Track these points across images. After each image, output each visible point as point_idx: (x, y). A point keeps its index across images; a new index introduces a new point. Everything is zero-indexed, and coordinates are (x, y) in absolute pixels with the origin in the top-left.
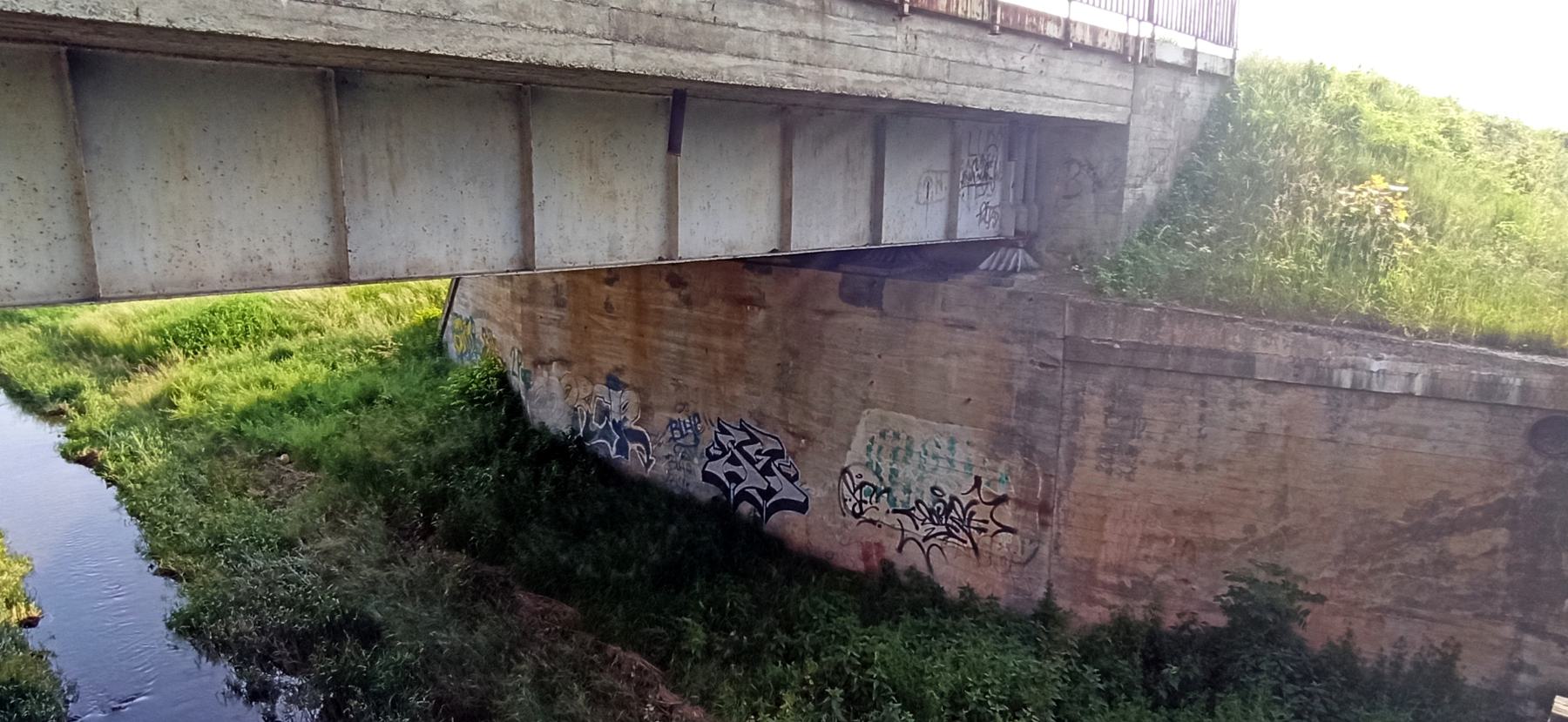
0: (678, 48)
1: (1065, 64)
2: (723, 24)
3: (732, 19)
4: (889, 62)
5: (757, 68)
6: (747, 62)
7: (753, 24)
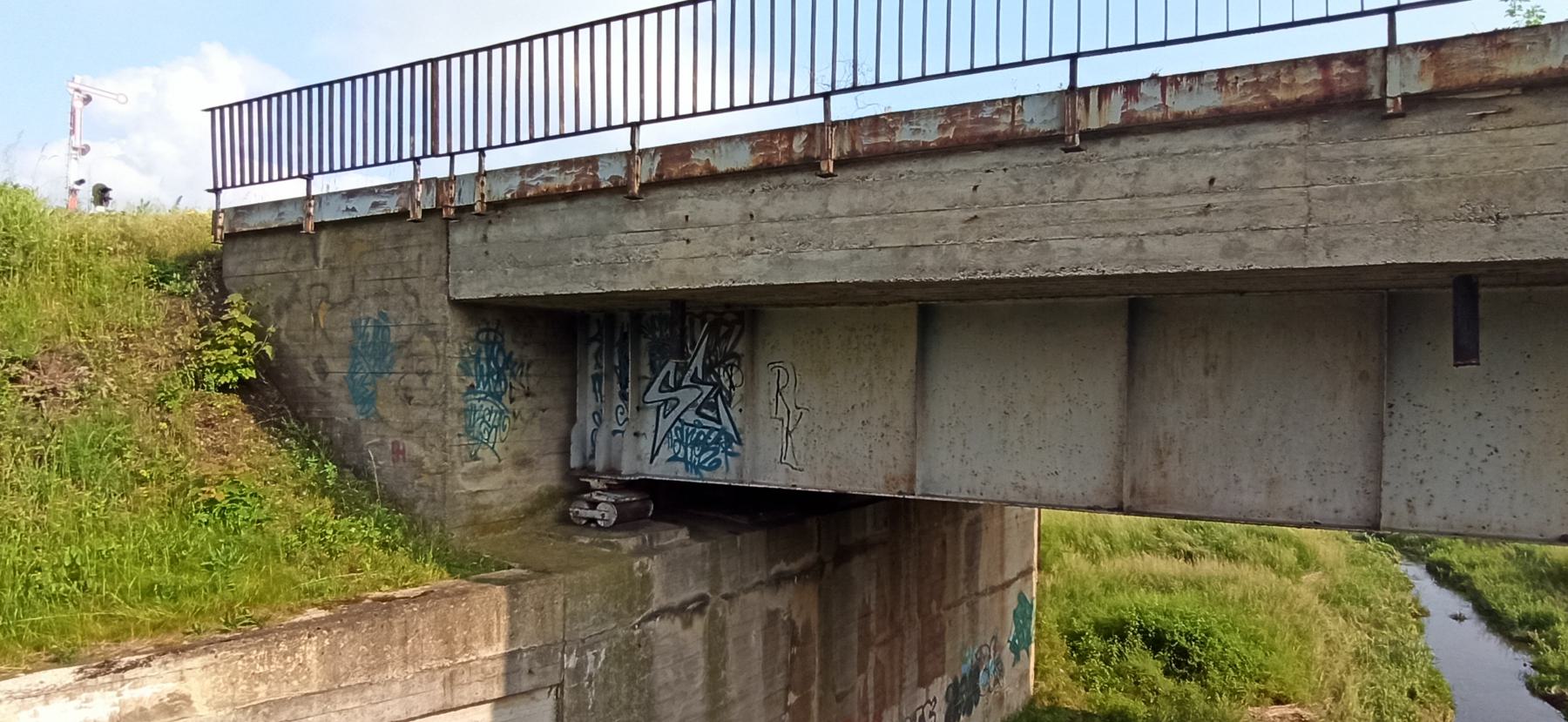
1: (1108, 175)
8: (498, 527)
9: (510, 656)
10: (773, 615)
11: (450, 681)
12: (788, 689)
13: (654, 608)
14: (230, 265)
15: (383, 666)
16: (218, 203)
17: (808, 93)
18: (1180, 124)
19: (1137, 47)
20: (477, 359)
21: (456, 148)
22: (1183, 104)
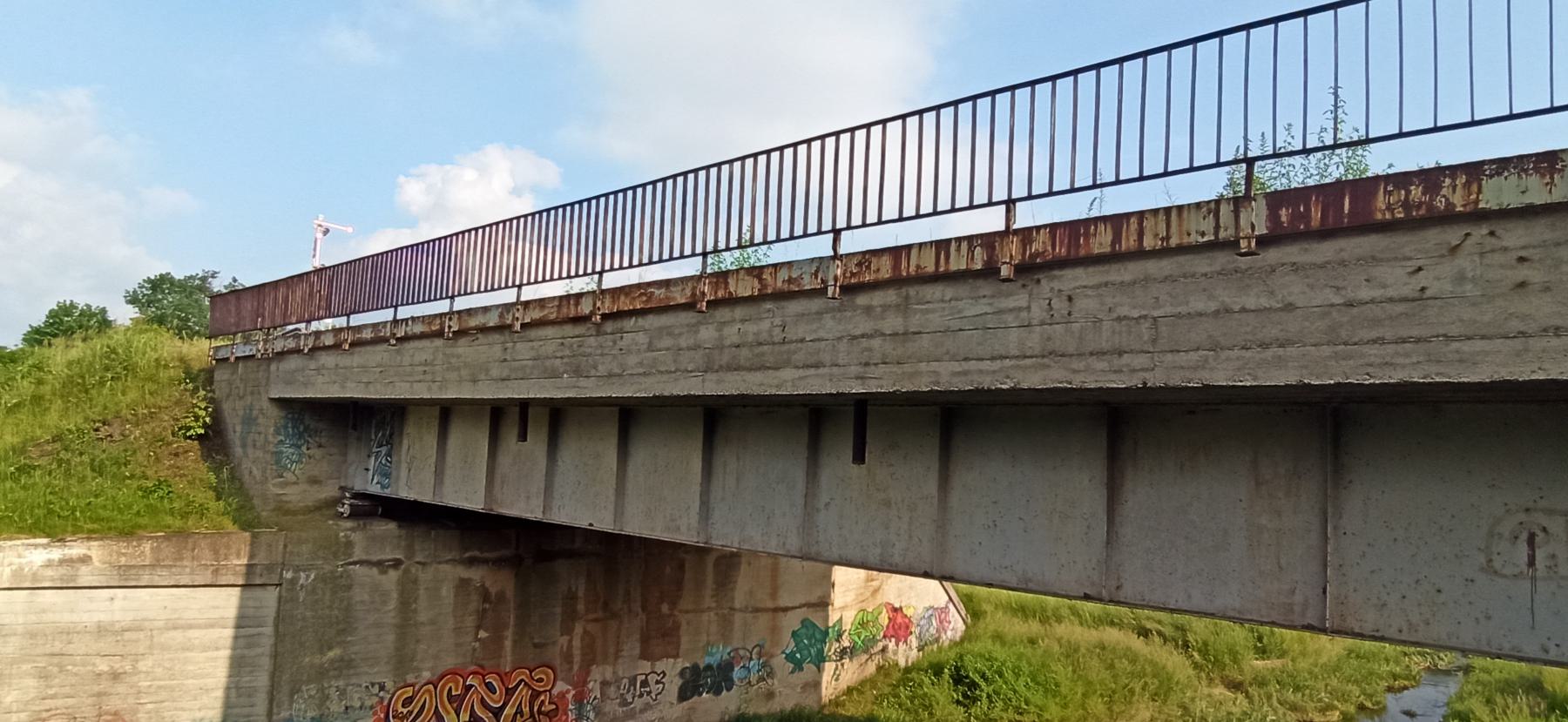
0: (750, 369)
1: (635, 334)
2: (791, 342)
3: (800, 336)
4: (1012, 340)
5: (822, 376)
6: (812, 371)
7: (822, 334)
8: (295, 513)
9: (250, 567)
10: (463, 584)
11: (216, 572)
12: (478, 628)
13: (355, 559)
14: (217, 376)
15: (181, 559)
16: (519, 296)
17: (1113, 179)
18: (484, 330)
19: (1436, 129)
20: (286, 427)
21: (841, 224)
22: (1494, 194)
